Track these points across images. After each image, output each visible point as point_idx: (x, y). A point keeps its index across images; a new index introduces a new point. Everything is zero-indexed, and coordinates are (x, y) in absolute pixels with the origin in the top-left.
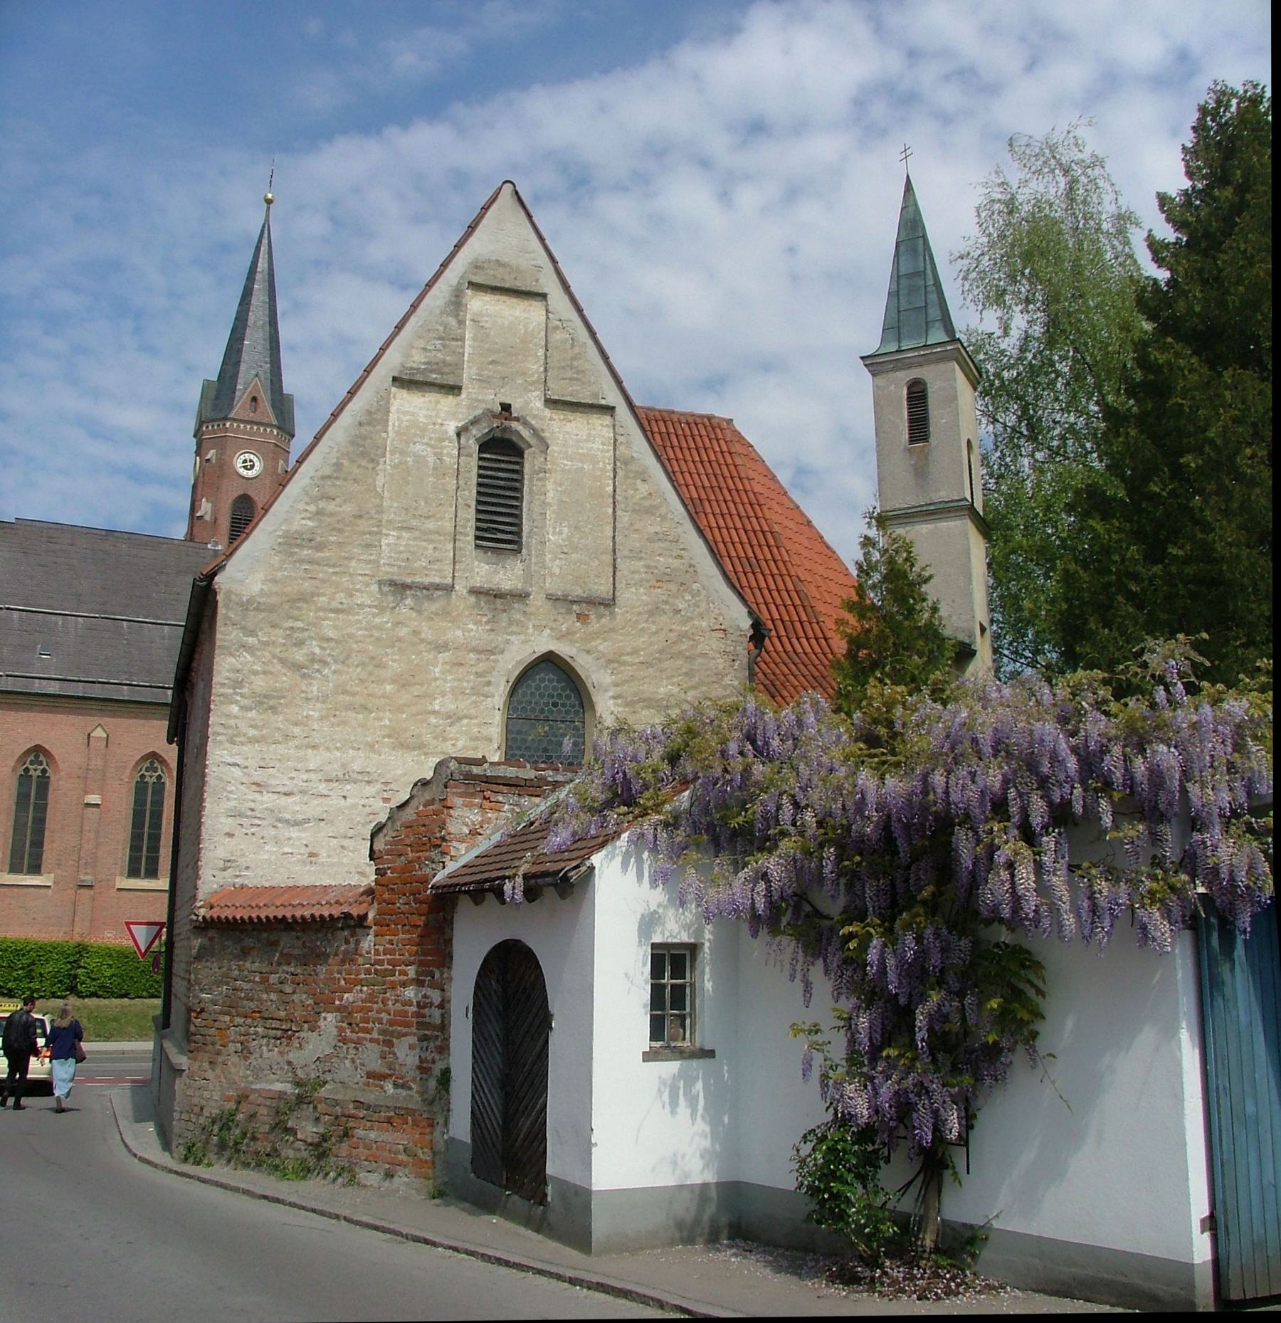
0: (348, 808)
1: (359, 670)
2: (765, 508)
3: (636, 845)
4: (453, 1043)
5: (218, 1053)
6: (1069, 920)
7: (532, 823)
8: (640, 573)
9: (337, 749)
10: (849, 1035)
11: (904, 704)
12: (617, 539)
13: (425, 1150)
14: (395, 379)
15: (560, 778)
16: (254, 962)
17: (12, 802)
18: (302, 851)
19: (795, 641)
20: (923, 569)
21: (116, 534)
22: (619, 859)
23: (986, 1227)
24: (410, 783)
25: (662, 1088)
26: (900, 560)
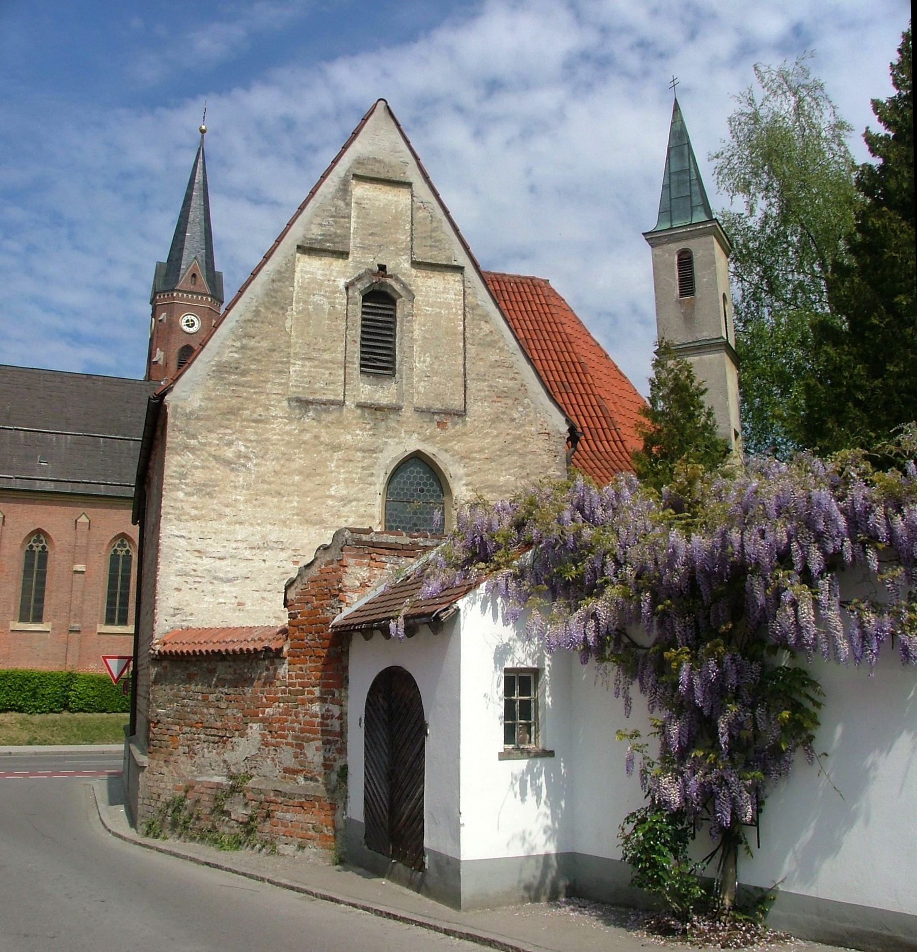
0: (266, 569)
1: (274, 463)
2: (574, 345)
3: (492, 592)
4: (350, 746)
5: (171, 754)
6: (844, 646)
7: (408, 578)
8: (485, 391)
9: (258, 524)
10: (663, 740)
11: (702, 478)
12: (467, 366)
13: (329, 828)
14: (299, 247)
15: (429, 543)
16: (197, 685)
17: (21, 570)
18: (233, 601)
19: (599, 443)
20: (700, 384)
21: (94, 377)
22: (479, 604)
23: (773, 890)
24: (314, 550)
25: (514, 782)
26: (682, 377)
